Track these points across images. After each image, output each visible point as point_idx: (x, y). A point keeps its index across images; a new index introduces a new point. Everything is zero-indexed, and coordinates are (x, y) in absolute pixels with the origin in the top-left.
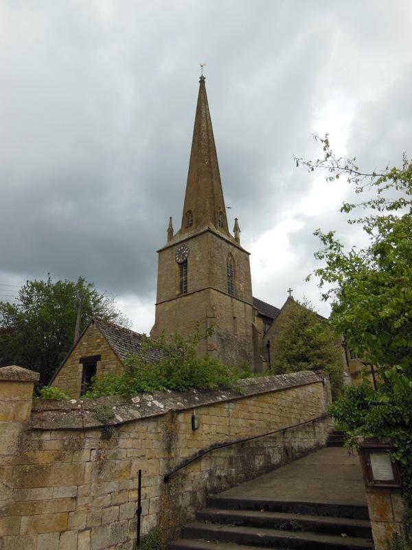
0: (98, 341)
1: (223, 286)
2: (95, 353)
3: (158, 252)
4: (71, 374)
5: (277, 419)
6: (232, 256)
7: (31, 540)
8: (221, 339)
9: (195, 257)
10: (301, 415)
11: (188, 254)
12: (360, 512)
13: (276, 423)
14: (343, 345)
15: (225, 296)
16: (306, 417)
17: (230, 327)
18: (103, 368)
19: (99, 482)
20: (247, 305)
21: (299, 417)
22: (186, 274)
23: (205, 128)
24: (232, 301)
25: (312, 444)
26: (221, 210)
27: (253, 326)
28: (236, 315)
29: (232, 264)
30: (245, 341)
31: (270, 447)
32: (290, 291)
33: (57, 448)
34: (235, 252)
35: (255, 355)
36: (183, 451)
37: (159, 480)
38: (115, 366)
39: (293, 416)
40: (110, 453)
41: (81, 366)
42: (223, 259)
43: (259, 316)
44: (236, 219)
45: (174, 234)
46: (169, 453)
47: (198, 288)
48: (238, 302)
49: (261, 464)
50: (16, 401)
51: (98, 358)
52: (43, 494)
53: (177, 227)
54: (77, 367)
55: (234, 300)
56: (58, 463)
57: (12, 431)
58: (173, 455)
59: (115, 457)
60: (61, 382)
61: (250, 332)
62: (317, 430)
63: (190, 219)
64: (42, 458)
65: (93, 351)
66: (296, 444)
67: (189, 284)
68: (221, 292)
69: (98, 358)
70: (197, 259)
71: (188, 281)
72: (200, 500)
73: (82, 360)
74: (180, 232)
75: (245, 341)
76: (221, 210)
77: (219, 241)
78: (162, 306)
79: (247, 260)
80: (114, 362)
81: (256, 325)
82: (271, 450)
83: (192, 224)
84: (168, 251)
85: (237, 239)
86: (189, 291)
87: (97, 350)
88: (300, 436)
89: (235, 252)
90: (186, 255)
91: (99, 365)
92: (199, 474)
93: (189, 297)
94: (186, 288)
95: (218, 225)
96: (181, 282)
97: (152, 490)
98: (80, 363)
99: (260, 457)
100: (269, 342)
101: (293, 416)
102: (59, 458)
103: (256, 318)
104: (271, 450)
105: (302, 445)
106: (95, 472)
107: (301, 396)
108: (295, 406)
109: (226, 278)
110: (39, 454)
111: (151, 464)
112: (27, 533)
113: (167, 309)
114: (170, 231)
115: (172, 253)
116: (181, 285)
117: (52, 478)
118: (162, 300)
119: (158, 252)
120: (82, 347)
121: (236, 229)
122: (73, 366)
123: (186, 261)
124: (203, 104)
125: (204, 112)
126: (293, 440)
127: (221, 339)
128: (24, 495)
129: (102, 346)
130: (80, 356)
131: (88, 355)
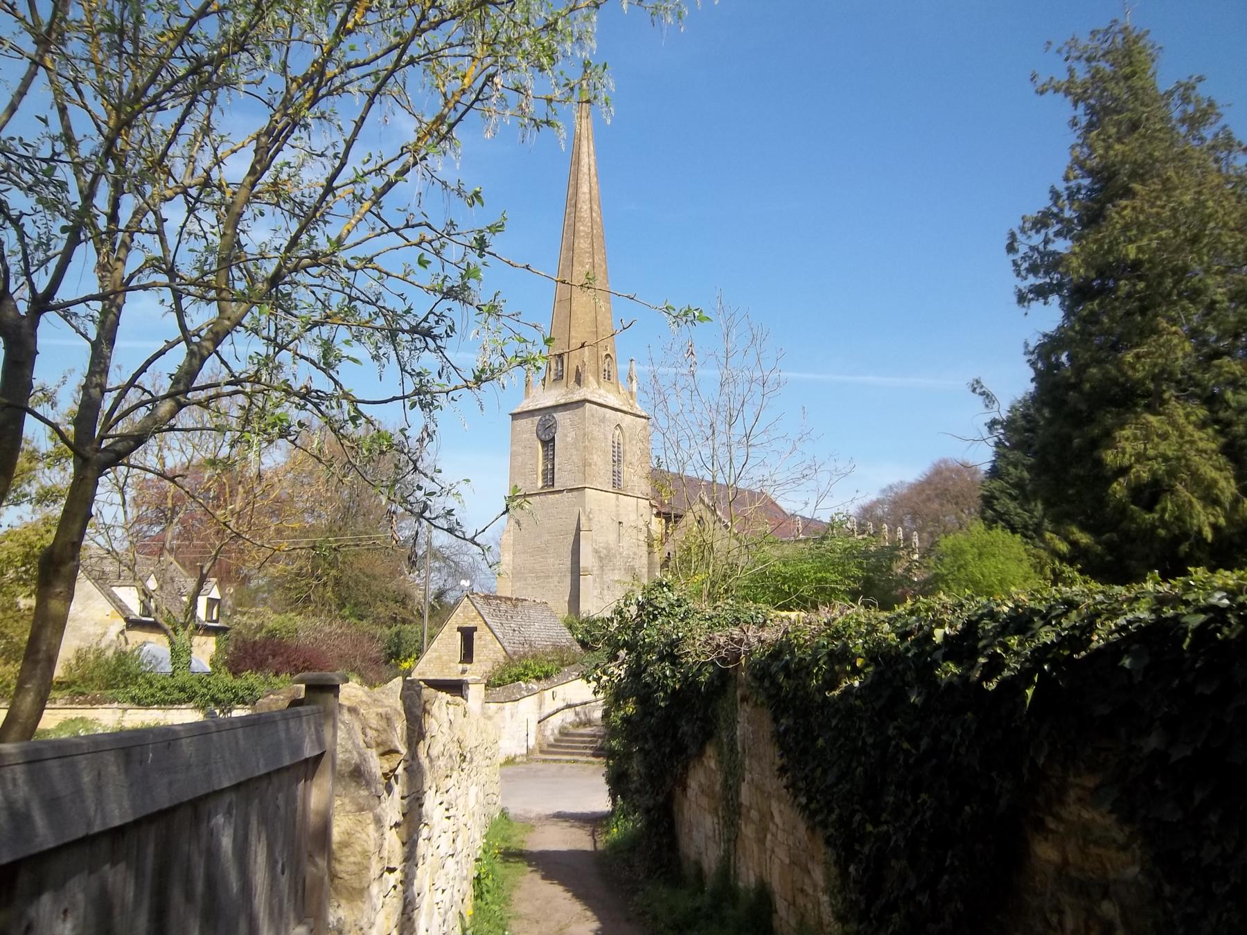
1: (605, 481)
2: (472, 624)
6: (621, 428)
8: (600, 557)
17: (612, 538)
23: (587, 196)
29: (621, 442)
30: (635, 554)
36: (548, 710)
41: (459, 633)
42: (606, 438)
51: (475, 629)
69: (475, 629)
70: (569, 439)
73: (459, 629)
75: (635, 554)
86: (557, 487)
91: (476, 635)
92: (556, 721)
97: (533, 726)
103: (653, 517)
127: (600, 557)
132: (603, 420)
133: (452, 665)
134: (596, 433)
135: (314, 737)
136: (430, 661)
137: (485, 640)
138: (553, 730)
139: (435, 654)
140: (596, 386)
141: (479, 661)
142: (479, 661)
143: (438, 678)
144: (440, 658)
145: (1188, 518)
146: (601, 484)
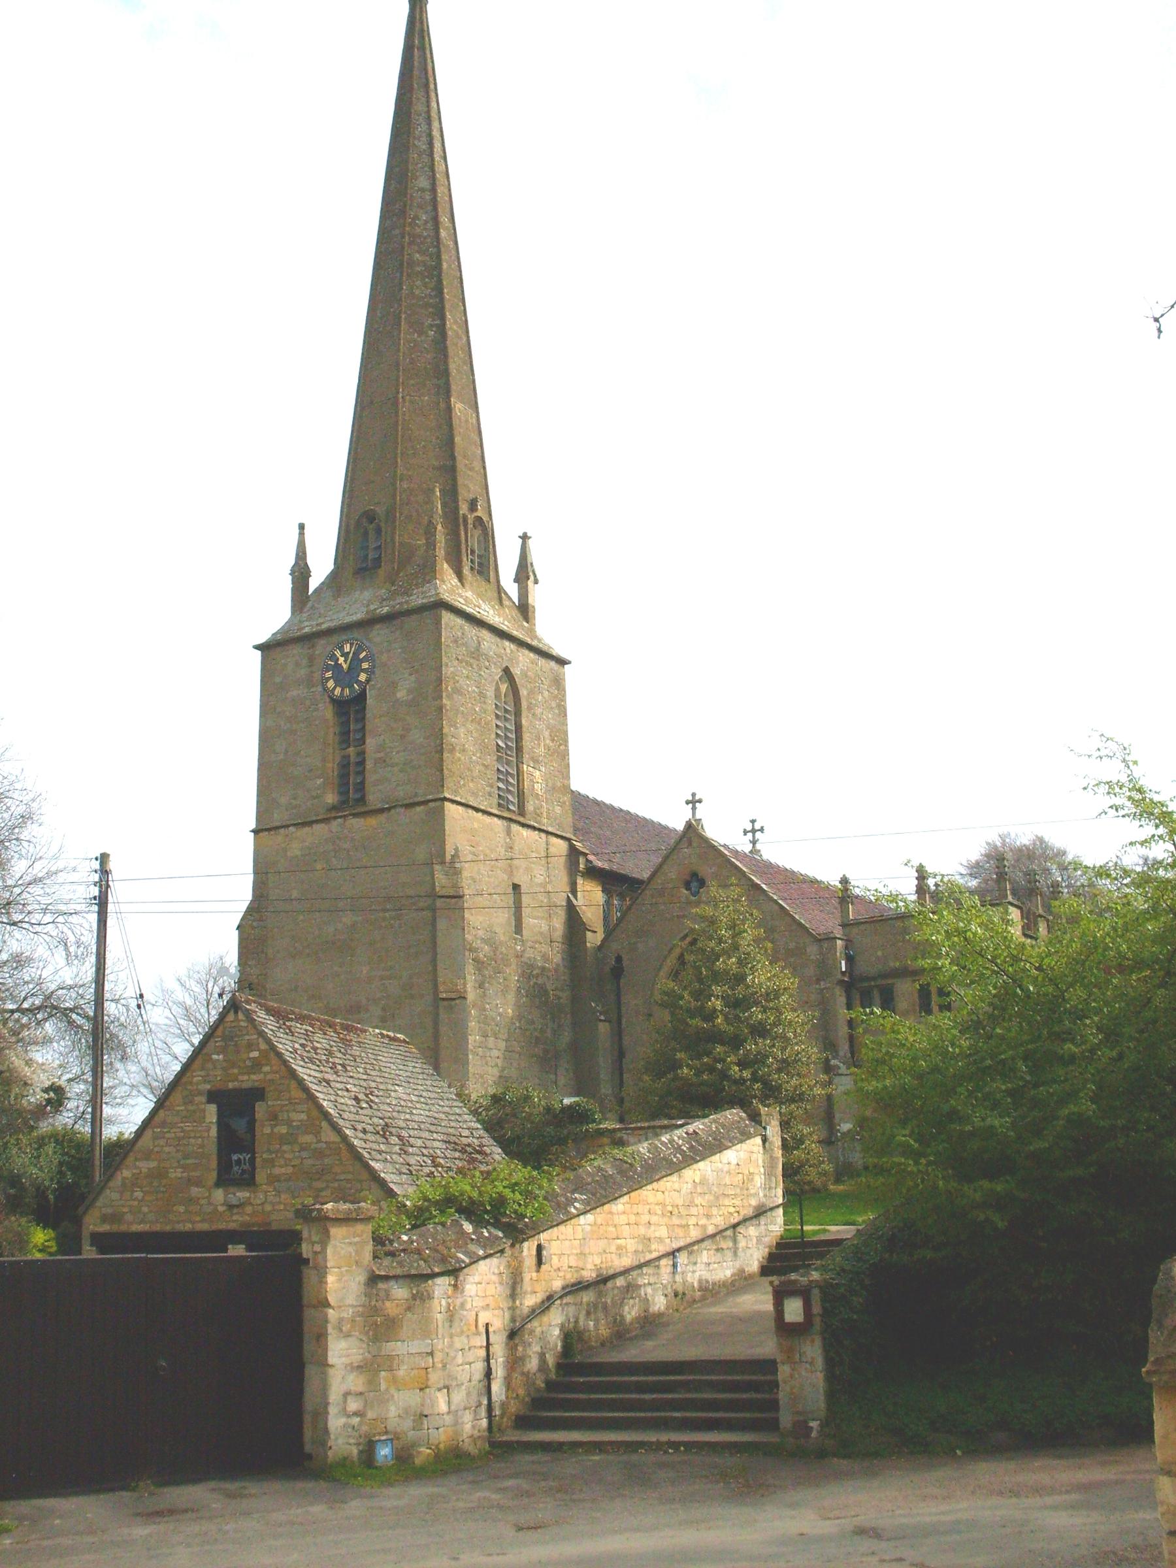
0: (255, 1054)
2: (249, 1080)
3: (257, 647)
4: (188, 1126)
5: (663, 1232)
7: (393, 1396)
9: (394, 685)
10: (708, 1216)
11: (370, 672)
12: (769, 1366)
13: (660, 1240)
14: (841, 982)
15: (488, 819)
16: (719, 1220)
18: (274, 1117)
19: (451, 1336)
20: (554, 840)
21: (703, 1221)
22: (362, 741)
24: (508, 832)
25: (728, 1273)
26: (480, 513)
27: (571, 909)
28: (521, 879)
31: (650, 1284)
32: (694, 802)
33: (406, 1296)
34: (523, 662)
35: (574, 999)
37: (505, 1335)
38: (303, 1116)
39: (692, 1221)
40: (458, 1302)
41: (212, 1109)
43: (593, 873)
44: (525, 537)
45: (314, 583)
46: (514, 1301)
47: (402, 793)
48: (525, 832)
49: (633, 1313)
50: (356, 1244)
51: (258, 1094)
52: (397, 1348)
53: (321, 566)
54: (204, 1111)
55: (515, 828)
56: (409, 1315)
57: (357, 1279)
58: (518, 1302)
59: (463, 1305)
60: (162, 1142)
61: (559, 923)
62: (742, 1243)
63: (372, 545)
64: (391, 1308)
65: (240, 1078)
66: (697, 1274)
67: (371, 778)
68: (477, 810)
69: (258, 1094)
70: (401, 694)
71: (369, 765)
72: (550, 1365)
74: (334, 580)
76: (480, 513)
77: (471, 631)
78: (279, 838)
79: (558, 683)
80: (299, 1107)
81: (579, 902)
82: (649, 1290)
83: (377, 562)
84: (296, 650)
85: (524, 610)
86: (374, 797)
87: (253, 1077)
88: (705, 1260)
89: (523, 662)
90: (363, 677)
91: (261, 1109)
92: (552, 1326)
93: (372, 821)
94: (361, 787)
95: (466, 571)
96: (345, 765)
98: (209, 1101)
99: (631, 1301)
100: (619, 959)
101: (692, 1221)
102: (409, 1309)
104: (649, 1290)
105: (706, 1275)
106: (447, 1325)
107: (711, 1177)
108: (698, 1200)
109: (491, 760)
110: (388, 1304)
111: (567, 1304)
112: (387, 1389)
113: (295, 850)
114: (301, 573)
115: (311, 659)
116: (344, 776)
117: (405, 1331)
118: (277, 818)
119: (257, 647)
120: (210, 1066)
121: (524, 573)
122: (191, 1108)
123: (362, 696)
124: (419, 94)
125: (419, 107)
126: (690, 1268)
128: (380, 1349)
129: (266, 1069)
130: (208, 1087)
131: (231, 1085)
132: (477, 653)
133: (195, 1191)
134: (463, 682)
135: (188, 1074)
136: (135, 1183)
137: (289, 1122)
138: (542, 1356)
139: (145, 1166)
140: (455, 581)
141: (273, 1180)
142: (273, 1180)
143: (158, 1228)
144: (159, 1174)
145: (471, 1478)
146: (474, 794)
